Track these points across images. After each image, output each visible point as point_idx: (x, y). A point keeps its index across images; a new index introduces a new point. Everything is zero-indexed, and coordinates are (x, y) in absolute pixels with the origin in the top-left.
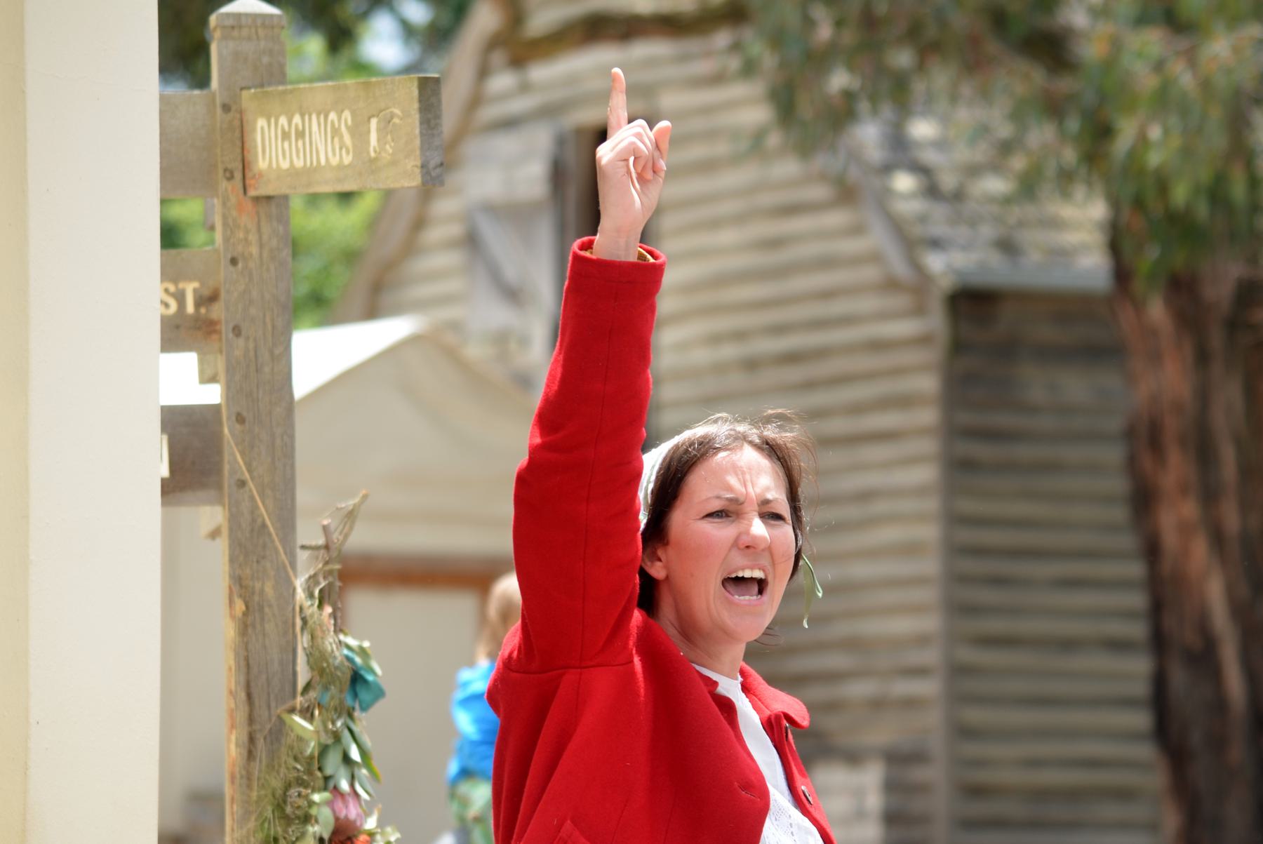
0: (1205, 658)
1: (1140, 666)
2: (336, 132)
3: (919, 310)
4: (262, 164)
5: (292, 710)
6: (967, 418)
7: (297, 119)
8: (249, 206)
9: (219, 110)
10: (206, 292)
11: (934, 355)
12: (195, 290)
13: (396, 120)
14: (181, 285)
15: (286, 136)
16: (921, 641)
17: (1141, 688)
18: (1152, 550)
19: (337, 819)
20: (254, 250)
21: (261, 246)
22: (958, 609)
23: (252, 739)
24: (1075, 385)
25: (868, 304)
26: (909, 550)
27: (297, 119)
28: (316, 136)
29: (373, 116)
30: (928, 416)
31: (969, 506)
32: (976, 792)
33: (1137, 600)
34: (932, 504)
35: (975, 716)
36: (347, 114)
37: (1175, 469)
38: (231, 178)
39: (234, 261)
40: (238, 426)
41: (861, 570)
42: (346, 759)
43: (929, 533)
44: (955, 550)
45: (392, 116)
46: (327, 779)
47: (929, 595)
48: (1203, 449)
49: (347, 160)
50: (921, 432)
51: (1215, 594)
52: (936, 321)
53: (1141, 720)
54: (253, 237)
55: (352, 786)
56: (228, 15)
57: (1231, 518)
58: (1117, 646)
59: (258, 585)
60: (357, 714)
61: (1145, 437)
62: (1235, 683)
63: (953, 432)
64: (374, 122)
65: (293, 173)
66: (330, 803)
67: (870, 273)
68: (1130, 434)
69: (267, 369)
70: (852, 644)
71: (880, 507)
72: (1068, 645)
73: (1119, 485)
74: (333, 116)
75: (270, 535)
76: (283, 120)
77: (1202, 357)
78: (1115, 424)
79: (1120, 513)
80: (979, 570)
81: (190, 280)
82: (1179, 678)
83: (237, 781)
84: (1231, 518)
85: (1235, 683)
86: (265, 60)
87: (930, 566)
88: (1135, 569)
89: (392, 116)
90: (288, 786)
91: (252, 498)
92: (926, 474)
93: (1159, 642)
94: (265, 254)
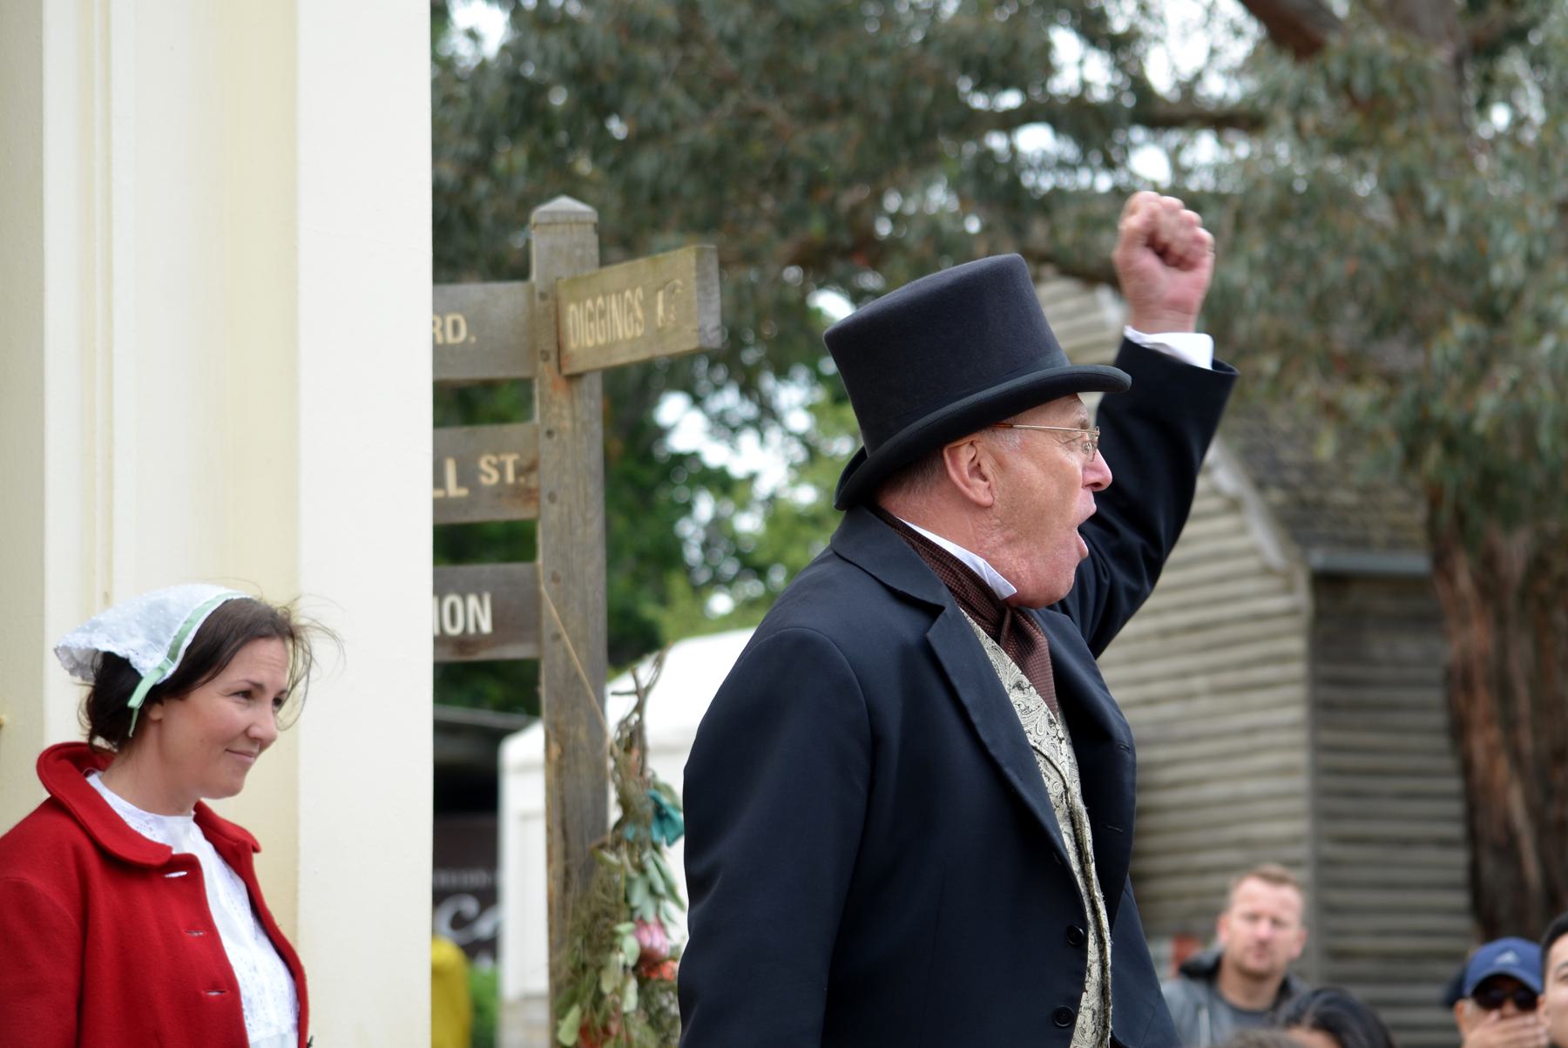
0: (1508, 849)
1: (1460, 857)
2: (631, 309)
3: (1288, 589)
4: (572, 345)
5: (602, 846)
6: (1327, 670)
7: (600, 301)
8: (562, 383)
9: (537, 299)
10: (525, 463)
11: (1301, 622)
12: (515, 463)
13: (678, 291)
14: (502, 458)
15: (591, 317)
16: (1295, 840)
17: (1460, 875)
18: (1466, 768)
19: (642, 948)
20: (567, 424)
21: (574, 419)
22: (1322, 815)
23: (567, 873)
24: (1410, 647)
25: (1251, 585)
26: (1286, 771)
27: (600, 301)
28: (615, 314)
29: (657, 290)
30: (1298, 669)
31: (1329, 737)
32: (1338, 955)
33: (1456, 808)
34: (1300, 736)
35: (1338, 897)
36: (639, 291)
37: (1483, 704)
38: (546, 359)
39: (550, 434)
40: (553, 585)
41: (1251, 787)
42: (652, 891)
43: (1300, 758)
44: (1320, 771)
45: (675, 287)
46: (632, 910)
47: (1300, 805)
48: (1503, 689)
49: (639, 332)
50: (1292, 682)
51: (1516, 802)
52: (1302, 598)
53: (1460, 899)
54: (566, 412)
55: (657, 915)
56: (545, 213)
57: (1527, 742)
58: (1444, 843)
59: (572, 730)
60: (664, 847)
61: (1459, 681)
62: (1532, 870)
63: (1317, 680)
64: (660, 295)
65: (598, 349)
66: (636, 933)
67: (1251, 563)
68: (1449, 676)
69: (579, 532)
70: (1243, 844)
71: (1262, 739)
72: (1407, 842)
73: (1438, 719)
74: (628, 294)
75: (582, 684)
76: (589, 303)
77: (1501, 620)
78: (1435, 674)
79: (1442, 742)
80: (1338, 787)
81: (510, 452)
82: (1489, 866)
83: (555, 910)
84: (1527, 742)
85: (1532, 870)
86: (578, 252)
87: (1300, 783)
88: (1454, 784)
89: (675, 287)
90: (595, 917)
91: (566, 651)
92: (1296, 713)
93: (1473, 838)
94: (578, 426)
